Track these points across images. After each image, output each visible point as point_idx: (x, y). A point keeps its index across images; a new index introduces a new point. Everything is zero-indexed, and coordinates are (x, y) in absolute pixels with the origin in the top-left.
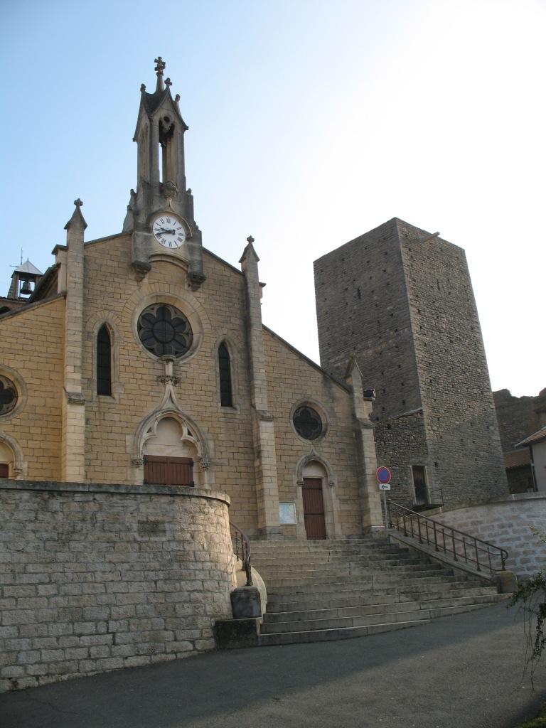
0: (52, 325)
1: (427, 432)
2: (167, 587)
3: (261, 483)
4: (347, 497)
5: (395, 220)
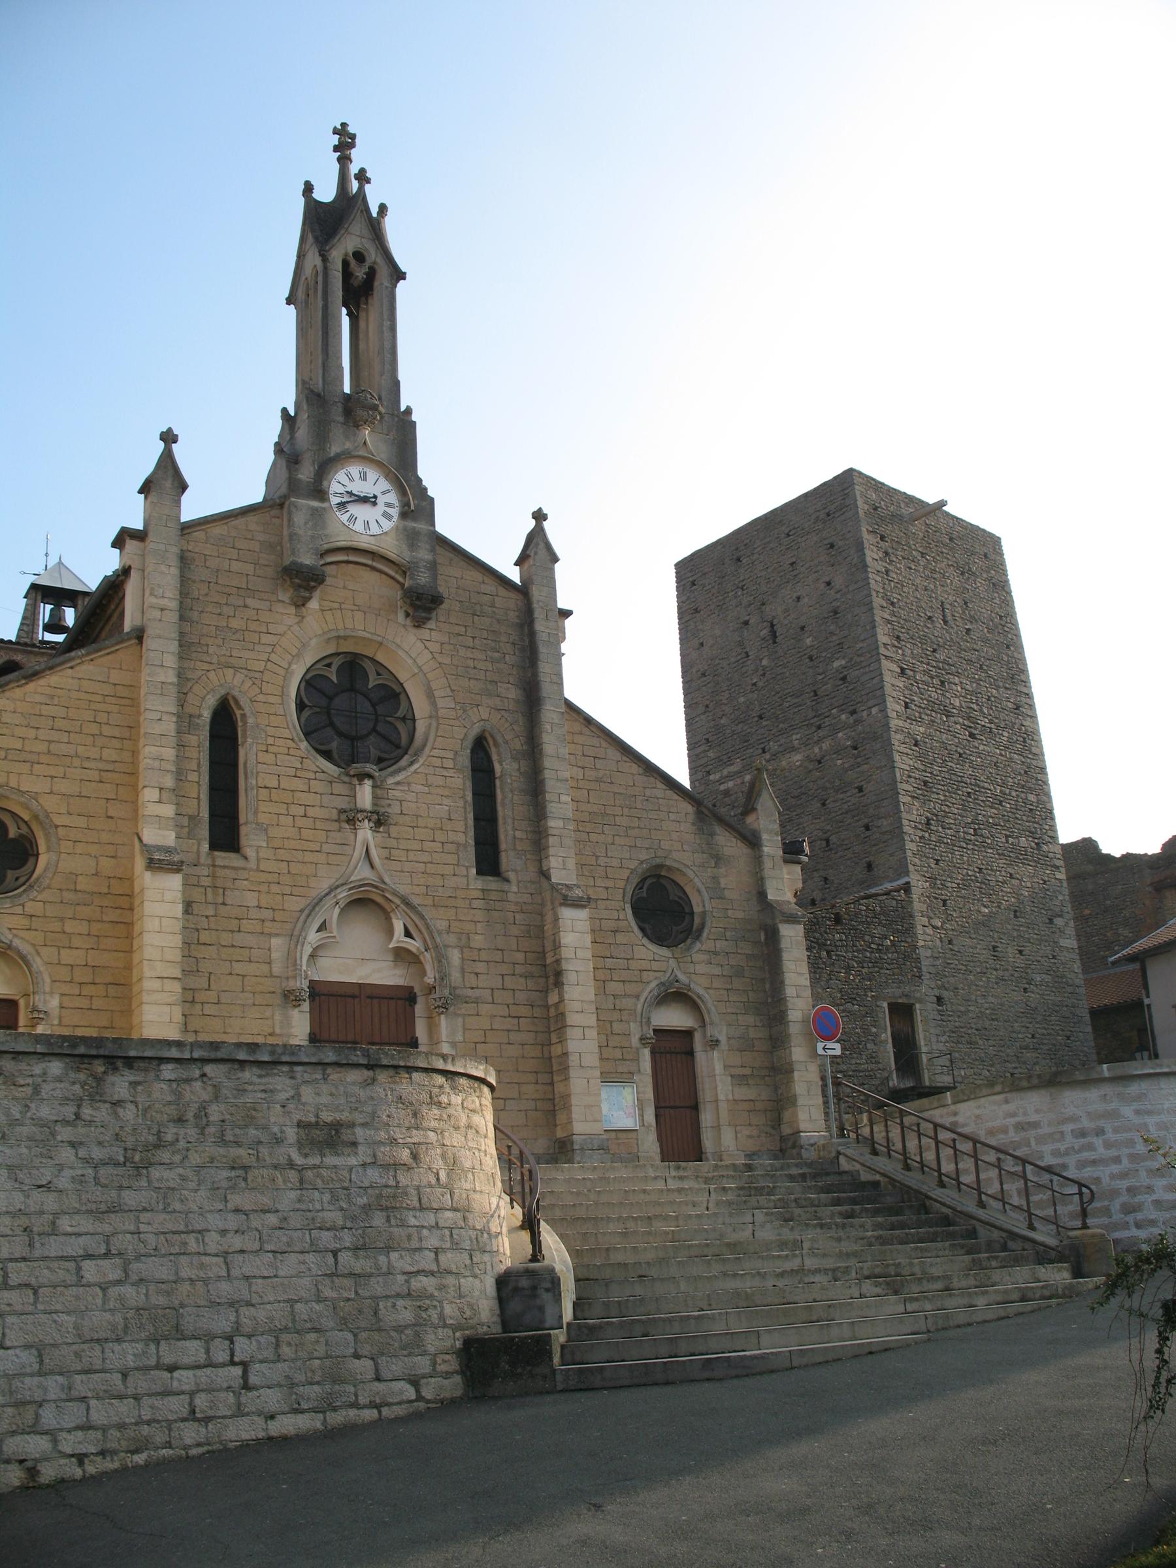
0: (113, 700)
2: (361, 1264)
4: (748, 1071)
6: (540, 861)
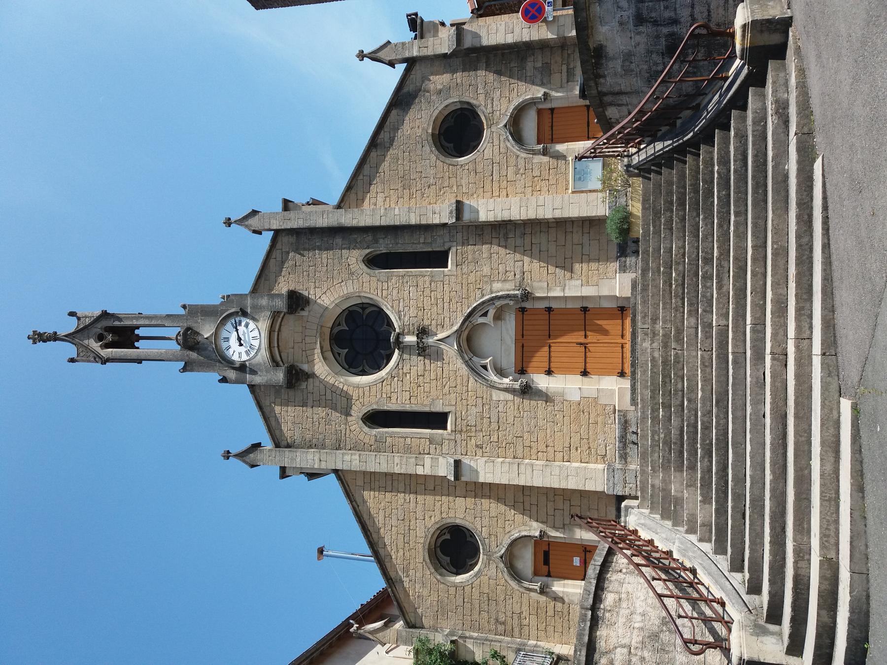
0: (372, 484)
4: (564, 67)
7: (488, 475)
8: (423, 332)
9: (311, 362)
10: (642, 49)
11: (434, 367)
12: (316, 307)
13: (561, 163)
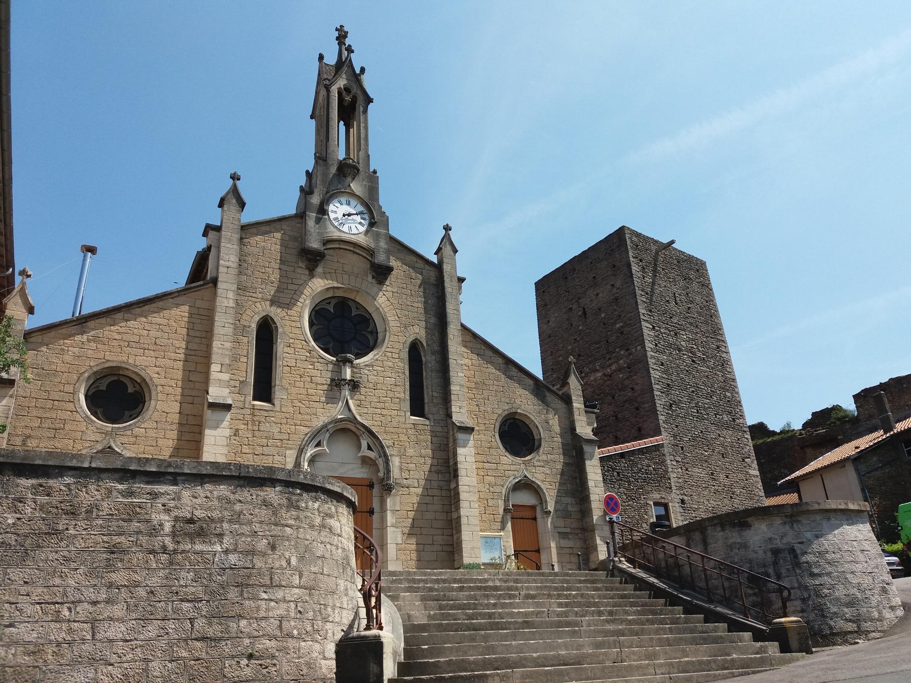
0: (197, 317)
1: (669, 462)
2: (214, 630)
3: (458, 508)
4: (568, 530)
5: (623, 227)
6: (447, 409)
7: (213, 439)
8: (354, 386)
9: (324, 276)
10: (752, 555)
11: (320, 393)
12: (375, 290)
13: (498, 525)
